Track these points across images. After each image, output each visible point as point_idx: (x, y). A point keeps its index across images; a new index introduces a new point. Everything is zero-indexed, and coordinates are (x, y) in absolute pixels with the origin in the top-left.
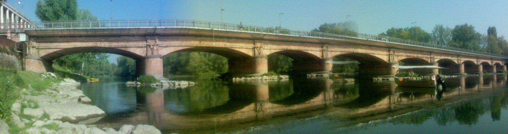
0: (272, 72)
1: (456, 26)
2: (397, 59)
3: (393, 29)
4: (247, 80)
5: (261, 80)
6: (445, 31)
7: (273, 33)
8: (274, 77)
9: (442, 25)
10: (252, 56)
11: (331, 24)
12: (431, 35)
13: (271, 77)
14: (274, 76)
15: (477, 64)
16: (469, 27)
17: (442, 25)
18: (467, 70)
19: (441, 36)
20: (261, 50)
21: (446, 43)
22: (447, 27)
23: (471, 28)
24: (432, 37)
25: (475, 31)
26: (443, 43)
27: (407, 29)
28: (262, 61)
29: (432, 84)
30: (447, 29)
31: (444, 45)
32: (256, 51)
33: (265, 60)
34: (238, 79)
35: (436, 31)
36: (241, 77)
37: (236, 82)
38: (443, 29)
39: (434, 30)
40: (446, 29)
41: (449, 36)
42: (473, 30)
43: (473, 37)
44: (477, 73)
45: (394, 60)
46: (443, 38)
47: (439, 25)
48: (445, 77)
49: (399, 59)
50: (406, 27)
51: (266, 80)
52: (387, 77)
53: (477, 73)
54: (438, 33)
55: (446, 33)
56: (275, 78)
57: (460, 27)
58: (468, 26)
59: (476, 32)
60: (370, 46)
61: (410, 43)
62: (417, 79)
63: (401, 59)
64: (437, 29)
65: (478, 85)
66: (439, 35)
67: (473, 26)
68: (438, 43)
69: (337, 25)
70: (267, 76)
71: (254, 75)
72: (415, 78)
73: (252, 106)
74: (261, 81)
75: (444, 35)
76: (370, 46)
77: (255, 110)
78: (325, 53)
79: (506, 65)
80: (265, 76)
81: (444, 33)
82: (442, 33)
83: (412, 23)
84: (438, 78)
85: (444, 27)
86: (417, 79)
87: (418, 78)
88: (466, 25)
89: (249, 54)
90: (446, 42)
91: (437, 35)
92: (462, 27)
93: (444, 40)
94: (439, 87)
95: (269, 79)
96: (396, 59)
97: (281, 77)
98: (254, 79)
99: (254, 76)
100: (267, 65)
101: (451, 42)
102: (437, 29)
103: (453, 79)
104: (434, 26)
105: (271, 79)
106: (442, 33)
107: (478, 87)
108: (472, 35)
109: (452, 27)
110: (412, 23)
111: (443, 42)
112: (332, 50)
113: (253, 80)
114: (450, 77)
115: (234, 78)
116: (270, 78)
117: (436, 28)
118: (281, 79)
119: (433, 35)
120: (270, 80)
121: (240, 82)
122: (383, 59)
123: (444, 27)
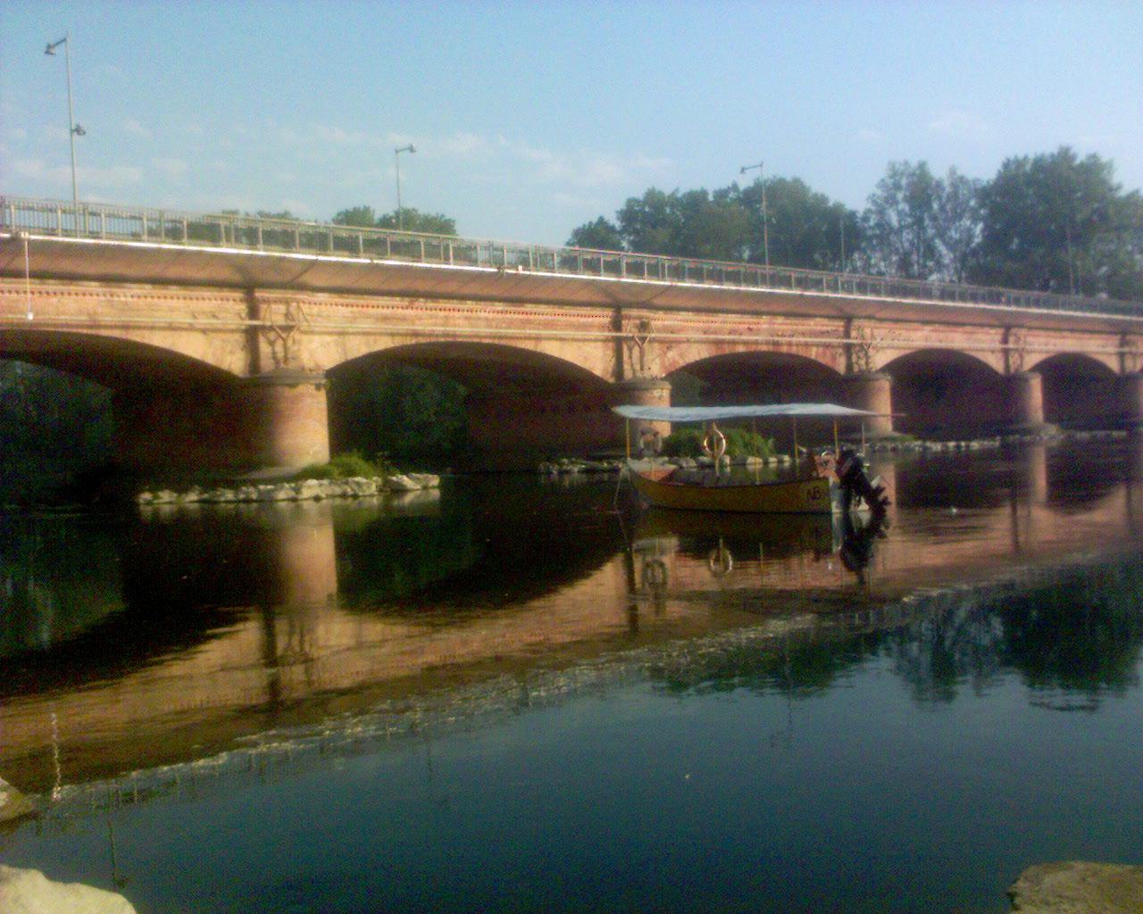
0: (355, 459)
1: (1006, 165)
2: (663, 365)
3: (653, 198)
4: (216, 503)
5: (294, 500)
6: (944, 195)
7: (474, 262)
8: (358, 484)
9: (922, 166)
10: (241, 375)
11: (679, 195)
12: (865, 219)
13: (347, 483)
14: (358, 479)
15: (1007, 366)
16: (1082, 165)
17: (922, 166)
18: (1055, 409)
19: (919, 222)
20: (290, 342)
21: (946, 261)
22: (953, 172)
23: (1093, 172)
24: (869, 233)
25: (1119, 187)
26: (930, 264)
27: (732, 195)
28: (298, 398)
29: (814, 498)
30: (954, 185)
31: (940, 271)
32: (264, 348)
33: (312, 396)
34: (166, 496)
35: (891, 200)
36: (181, 489)
37: (156, 513)
38: (928, 187)
39: (879, 192)
40: (946, 184)
41: (966, 222)
42: (1104, 182)
43: (1103, 217)
44: (1011, 427)
45: (642, 369)
46: (931, 232)
47: (906, 163)
48: (925, 449)
49: (674, 362)
50: (724, 184)
51: (317, 499)
52: (608, 458)
53: (1011, 427)
54: (904, 206)
55: (949, 207)
56: (368, 486)
57: (1028, 167)
58: (1078, 162)
59: (1123, 193)
60: (515, 293)
61: (636, 269)
62: (766, 463)
63: (682, 363)
64: (897, 187)
65: (1128, 488)
66: (909, 220)
67: (1104, 159)
68: (904, 265)
69: (711, 198)
70: (325, 482)
71: (255, 475)
72: (759, 460)
73: (249, 633)
74: (292, 505)
75: (934, 218)
76: (515, 293)
77: (270, 657)
78: (630, 350)
79: (671, 383)
80: (313, 482)
81: (935, 206)
82: (928, 205)
83: (743, 170)
84: (849, 463)
85: (939, 171)
86: (766, 463)
87: (773, 460)
88: (1065, 155)
89: (225, 366)
90: (947, 256)
91: (899, 222)
92: (1039, 164)
93: (938, 242)
94: (852, 508)
95: (333, 496)
96: (657, 361)
97: (398, 483)
98: (254, 496)
99: (254, 483)
100: (325, 421)
101: (974, 253)
102: (897, 187)
103: (969, 456)
104: (882, 173)
105: (344, 496)
106: (927, 204)
107: (1129, 500)
108: (1095, 211)
109: (985, 170)
110: (743, 170)
111: (930, 251)
112: (563, 336)
113: (248, 501)
114: (958, 447)
115: (142, 491)
116: (338, 490)
117: (890, 182)
118: (400, 491)
119: (872, 223)
120: (338, 501)
121: (181, 517)
122: (586, 365)
123: (939, 172)
